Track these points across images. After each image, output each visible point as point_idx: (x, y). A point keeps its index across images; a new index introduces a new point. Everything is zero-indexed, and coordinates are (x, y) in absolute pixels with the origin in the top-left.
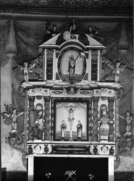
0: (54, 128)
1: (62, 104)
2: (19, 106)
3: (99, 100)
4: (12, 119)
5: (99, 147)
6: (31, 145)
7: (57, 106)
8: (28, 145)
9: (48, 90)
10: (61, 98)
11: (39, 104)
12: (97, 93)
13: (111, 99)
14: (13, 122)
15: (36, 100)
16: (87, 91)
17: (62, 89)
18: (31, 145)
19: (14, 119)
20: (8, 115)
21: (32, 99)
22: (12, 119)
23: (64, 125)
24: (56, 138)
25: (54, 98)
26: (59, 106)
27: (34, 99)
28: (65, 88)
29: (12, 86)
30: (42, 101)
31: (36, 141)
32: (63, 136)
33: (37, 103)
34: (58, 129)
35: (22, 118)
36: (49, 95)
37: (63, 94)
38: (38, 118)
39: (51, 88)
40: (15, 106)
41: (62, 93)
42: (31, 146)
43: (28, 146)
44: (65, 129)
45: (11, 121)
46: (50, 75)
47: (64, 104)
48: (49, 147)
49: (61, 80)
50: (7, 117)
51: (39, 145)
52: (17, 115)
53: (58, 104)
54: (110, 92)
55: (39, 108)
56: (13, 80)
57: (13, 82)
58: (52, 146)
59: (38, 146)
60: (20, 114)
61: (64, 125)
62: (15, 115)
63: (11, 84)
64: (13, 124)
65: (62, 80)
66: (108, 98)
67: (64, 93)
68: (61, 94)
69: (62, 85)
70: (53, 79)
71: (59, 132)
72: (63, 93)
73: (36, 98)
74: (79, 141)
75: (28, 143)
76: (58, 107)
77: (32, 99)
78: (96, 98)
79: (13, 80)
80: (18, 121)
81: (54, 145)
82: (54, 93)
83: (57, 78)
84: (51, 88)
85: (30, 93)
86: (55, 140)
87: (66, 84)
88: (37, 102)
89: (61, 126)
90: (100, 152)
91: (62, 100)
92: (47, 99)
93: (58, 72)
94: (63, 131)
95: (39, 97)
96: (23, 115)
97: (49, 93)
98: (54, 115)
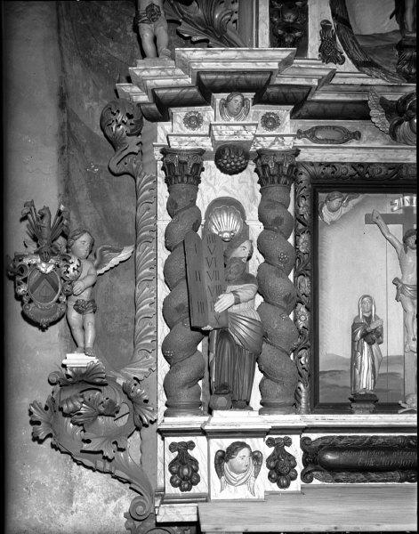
0: (311, 337)
1: (361, 196)
2: (106, 216)
3: (203, 175)
4: (68, 287)
5: (203, 451)
6: (187, 439)
7: (326, 215)
8: (169, 440)
9: (284, 112)
10: (353, 165)
11: (227, 204)
12: (194, 127)
13: (279, 165)
14: (71, 304)
15: (210, 169)
16: (337, 122)
17: (365, 116)
18: (187, 439)
19: (78, 286)
20: (46, 261)
21: (184, 171)
22: (68, 287)
23: (369, 319)
24: (322, 399)
25: (312, 164)
26: (335, 217)
27: (199, 168)
28: (383, 103)
29: (62, 105)
30: (244, 187)
31: (225, 418)
32: (365, 381)
33: (213, 197)
34: (335, 342)
35: (124, 288)
36: (289, 143)
37: (363, 145)
38: (228, 281)
39: (298, 101)
40: (79, 218)
41: (357, 135)
42: (191, 445)
43: (173, 447)
44: (374, 347)
45: (63, 299)
46: (289, 28)
47: (363, 201)
48: (295, 449)
49: (348, 66)
50: (36, 275)
51: (248, 441)
52: (97, 268)
53: (335, 203)
54: (270, 122)
55: (226, 225)
56: (63, 70)
57: (63, 81)
58: (305, 443)
59: (244, 452)
60: (114, 261)
61: (369, 319)
62: (87, 266)
63: (56, 91)
64: (74, 316)
65: (355, 62)
66: (260, 154)
67: (369, 138)
68: (354, 144)
69: (364, 89)
70: (310, 55)
71: (338, 360)
72: (364, 136)
73: (210, 164)
74: (364, 411)
75: (164, 433)
76: (333, 222)
77: (184, 171)
78: (278, 159)
79: (63, 70)
80: (99, 303)
81: (314, 436)
82: (311, 134)
83: (328, 53)
84: (298, 101)
85: (174, 133)
86: (316, 406)
87: (380, 81)
88: (214, 184)
89: (355, 326)
90: (208, 480)
91: (361, 181)
92: (276, 172)
93: (333, 14)
94: (365, 360)
95: (230, 158)
96: (132, 263)
97: (283, 133)
98: (310, 266)
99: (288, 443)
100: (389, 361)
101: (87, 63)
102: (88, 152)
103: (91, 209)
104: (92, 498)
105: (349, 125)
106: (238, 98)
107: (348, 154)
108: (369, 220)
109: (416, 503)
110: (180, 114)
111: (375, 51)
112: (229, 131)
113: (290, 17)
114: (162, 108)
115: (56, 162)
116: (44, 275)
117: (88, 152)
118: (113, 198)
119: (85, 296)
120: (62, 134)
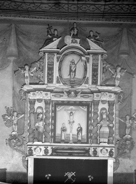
0: (54, 130)
3: (36, 103)
4: (13, 121)
7: (57, 109)
8: (28, 147)
9: (49, 93)
10: (62, 101)
11: (40, 107)
17: (63, 93)
19: (14, 121)
20: (9, 117)
21: (32, 102)
23: (64, 127)
24: (56, 141)
26: (59, 110)
27: (35, 102)
28: (66, 91)
30: (42, 104)
32: (63, 138)
33: (38, 106)
34: (58, 131)
35: (23, 121)
39: (51, 91)
41: (63, 96)
46: (50, 79)
48: (49, 148)
49: (61, 84)
51: (39, 147)
53: (59, 107)
55: (39, 111)
58: (52, 148)
59: (38, 148)
60: (21, 117)
63: (12, 87)
68: (62, 97)
69: (63, 89)
70: (54, 83)
77: (32, 102)
80: (18, 123)
81: (54, 147)
82: (55, 96)
83: (58, 82)
84: (51, 91)
85: (31, 96)
86: (55, 142)
88: (37, 105)
89: (61, 128)
91: (63, 104)
92: (47, 103)
96: (24, 117)
98: (54, 118)
99: (48, 147)
100: (68, 135)
101: (18, 82)
102: (17, 97)
103: (18, 107)
104: (16, 157)
105: (61, 94)
106: (40, 92)
107: (61, 99)
108: (65, 110)
109: (108, 181)
110: (31, 93)
111: (66, 81)
112: (37, 97)
113: (50, 77)
114: (29, 92)
115: (12, 100)
116: (9, 119)
117: (17, 97)
118: (21, 105)
119: (16, 123)
120: (13, 95)
